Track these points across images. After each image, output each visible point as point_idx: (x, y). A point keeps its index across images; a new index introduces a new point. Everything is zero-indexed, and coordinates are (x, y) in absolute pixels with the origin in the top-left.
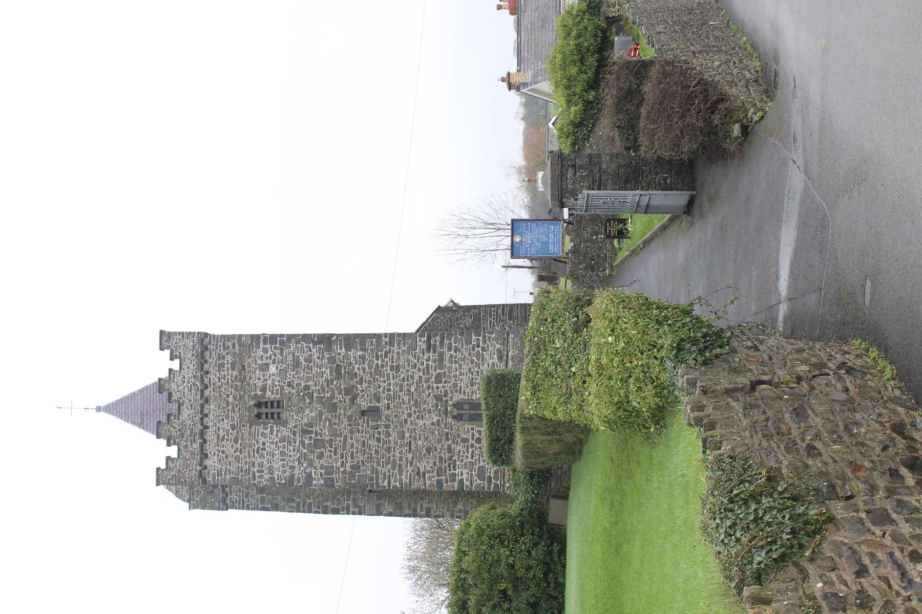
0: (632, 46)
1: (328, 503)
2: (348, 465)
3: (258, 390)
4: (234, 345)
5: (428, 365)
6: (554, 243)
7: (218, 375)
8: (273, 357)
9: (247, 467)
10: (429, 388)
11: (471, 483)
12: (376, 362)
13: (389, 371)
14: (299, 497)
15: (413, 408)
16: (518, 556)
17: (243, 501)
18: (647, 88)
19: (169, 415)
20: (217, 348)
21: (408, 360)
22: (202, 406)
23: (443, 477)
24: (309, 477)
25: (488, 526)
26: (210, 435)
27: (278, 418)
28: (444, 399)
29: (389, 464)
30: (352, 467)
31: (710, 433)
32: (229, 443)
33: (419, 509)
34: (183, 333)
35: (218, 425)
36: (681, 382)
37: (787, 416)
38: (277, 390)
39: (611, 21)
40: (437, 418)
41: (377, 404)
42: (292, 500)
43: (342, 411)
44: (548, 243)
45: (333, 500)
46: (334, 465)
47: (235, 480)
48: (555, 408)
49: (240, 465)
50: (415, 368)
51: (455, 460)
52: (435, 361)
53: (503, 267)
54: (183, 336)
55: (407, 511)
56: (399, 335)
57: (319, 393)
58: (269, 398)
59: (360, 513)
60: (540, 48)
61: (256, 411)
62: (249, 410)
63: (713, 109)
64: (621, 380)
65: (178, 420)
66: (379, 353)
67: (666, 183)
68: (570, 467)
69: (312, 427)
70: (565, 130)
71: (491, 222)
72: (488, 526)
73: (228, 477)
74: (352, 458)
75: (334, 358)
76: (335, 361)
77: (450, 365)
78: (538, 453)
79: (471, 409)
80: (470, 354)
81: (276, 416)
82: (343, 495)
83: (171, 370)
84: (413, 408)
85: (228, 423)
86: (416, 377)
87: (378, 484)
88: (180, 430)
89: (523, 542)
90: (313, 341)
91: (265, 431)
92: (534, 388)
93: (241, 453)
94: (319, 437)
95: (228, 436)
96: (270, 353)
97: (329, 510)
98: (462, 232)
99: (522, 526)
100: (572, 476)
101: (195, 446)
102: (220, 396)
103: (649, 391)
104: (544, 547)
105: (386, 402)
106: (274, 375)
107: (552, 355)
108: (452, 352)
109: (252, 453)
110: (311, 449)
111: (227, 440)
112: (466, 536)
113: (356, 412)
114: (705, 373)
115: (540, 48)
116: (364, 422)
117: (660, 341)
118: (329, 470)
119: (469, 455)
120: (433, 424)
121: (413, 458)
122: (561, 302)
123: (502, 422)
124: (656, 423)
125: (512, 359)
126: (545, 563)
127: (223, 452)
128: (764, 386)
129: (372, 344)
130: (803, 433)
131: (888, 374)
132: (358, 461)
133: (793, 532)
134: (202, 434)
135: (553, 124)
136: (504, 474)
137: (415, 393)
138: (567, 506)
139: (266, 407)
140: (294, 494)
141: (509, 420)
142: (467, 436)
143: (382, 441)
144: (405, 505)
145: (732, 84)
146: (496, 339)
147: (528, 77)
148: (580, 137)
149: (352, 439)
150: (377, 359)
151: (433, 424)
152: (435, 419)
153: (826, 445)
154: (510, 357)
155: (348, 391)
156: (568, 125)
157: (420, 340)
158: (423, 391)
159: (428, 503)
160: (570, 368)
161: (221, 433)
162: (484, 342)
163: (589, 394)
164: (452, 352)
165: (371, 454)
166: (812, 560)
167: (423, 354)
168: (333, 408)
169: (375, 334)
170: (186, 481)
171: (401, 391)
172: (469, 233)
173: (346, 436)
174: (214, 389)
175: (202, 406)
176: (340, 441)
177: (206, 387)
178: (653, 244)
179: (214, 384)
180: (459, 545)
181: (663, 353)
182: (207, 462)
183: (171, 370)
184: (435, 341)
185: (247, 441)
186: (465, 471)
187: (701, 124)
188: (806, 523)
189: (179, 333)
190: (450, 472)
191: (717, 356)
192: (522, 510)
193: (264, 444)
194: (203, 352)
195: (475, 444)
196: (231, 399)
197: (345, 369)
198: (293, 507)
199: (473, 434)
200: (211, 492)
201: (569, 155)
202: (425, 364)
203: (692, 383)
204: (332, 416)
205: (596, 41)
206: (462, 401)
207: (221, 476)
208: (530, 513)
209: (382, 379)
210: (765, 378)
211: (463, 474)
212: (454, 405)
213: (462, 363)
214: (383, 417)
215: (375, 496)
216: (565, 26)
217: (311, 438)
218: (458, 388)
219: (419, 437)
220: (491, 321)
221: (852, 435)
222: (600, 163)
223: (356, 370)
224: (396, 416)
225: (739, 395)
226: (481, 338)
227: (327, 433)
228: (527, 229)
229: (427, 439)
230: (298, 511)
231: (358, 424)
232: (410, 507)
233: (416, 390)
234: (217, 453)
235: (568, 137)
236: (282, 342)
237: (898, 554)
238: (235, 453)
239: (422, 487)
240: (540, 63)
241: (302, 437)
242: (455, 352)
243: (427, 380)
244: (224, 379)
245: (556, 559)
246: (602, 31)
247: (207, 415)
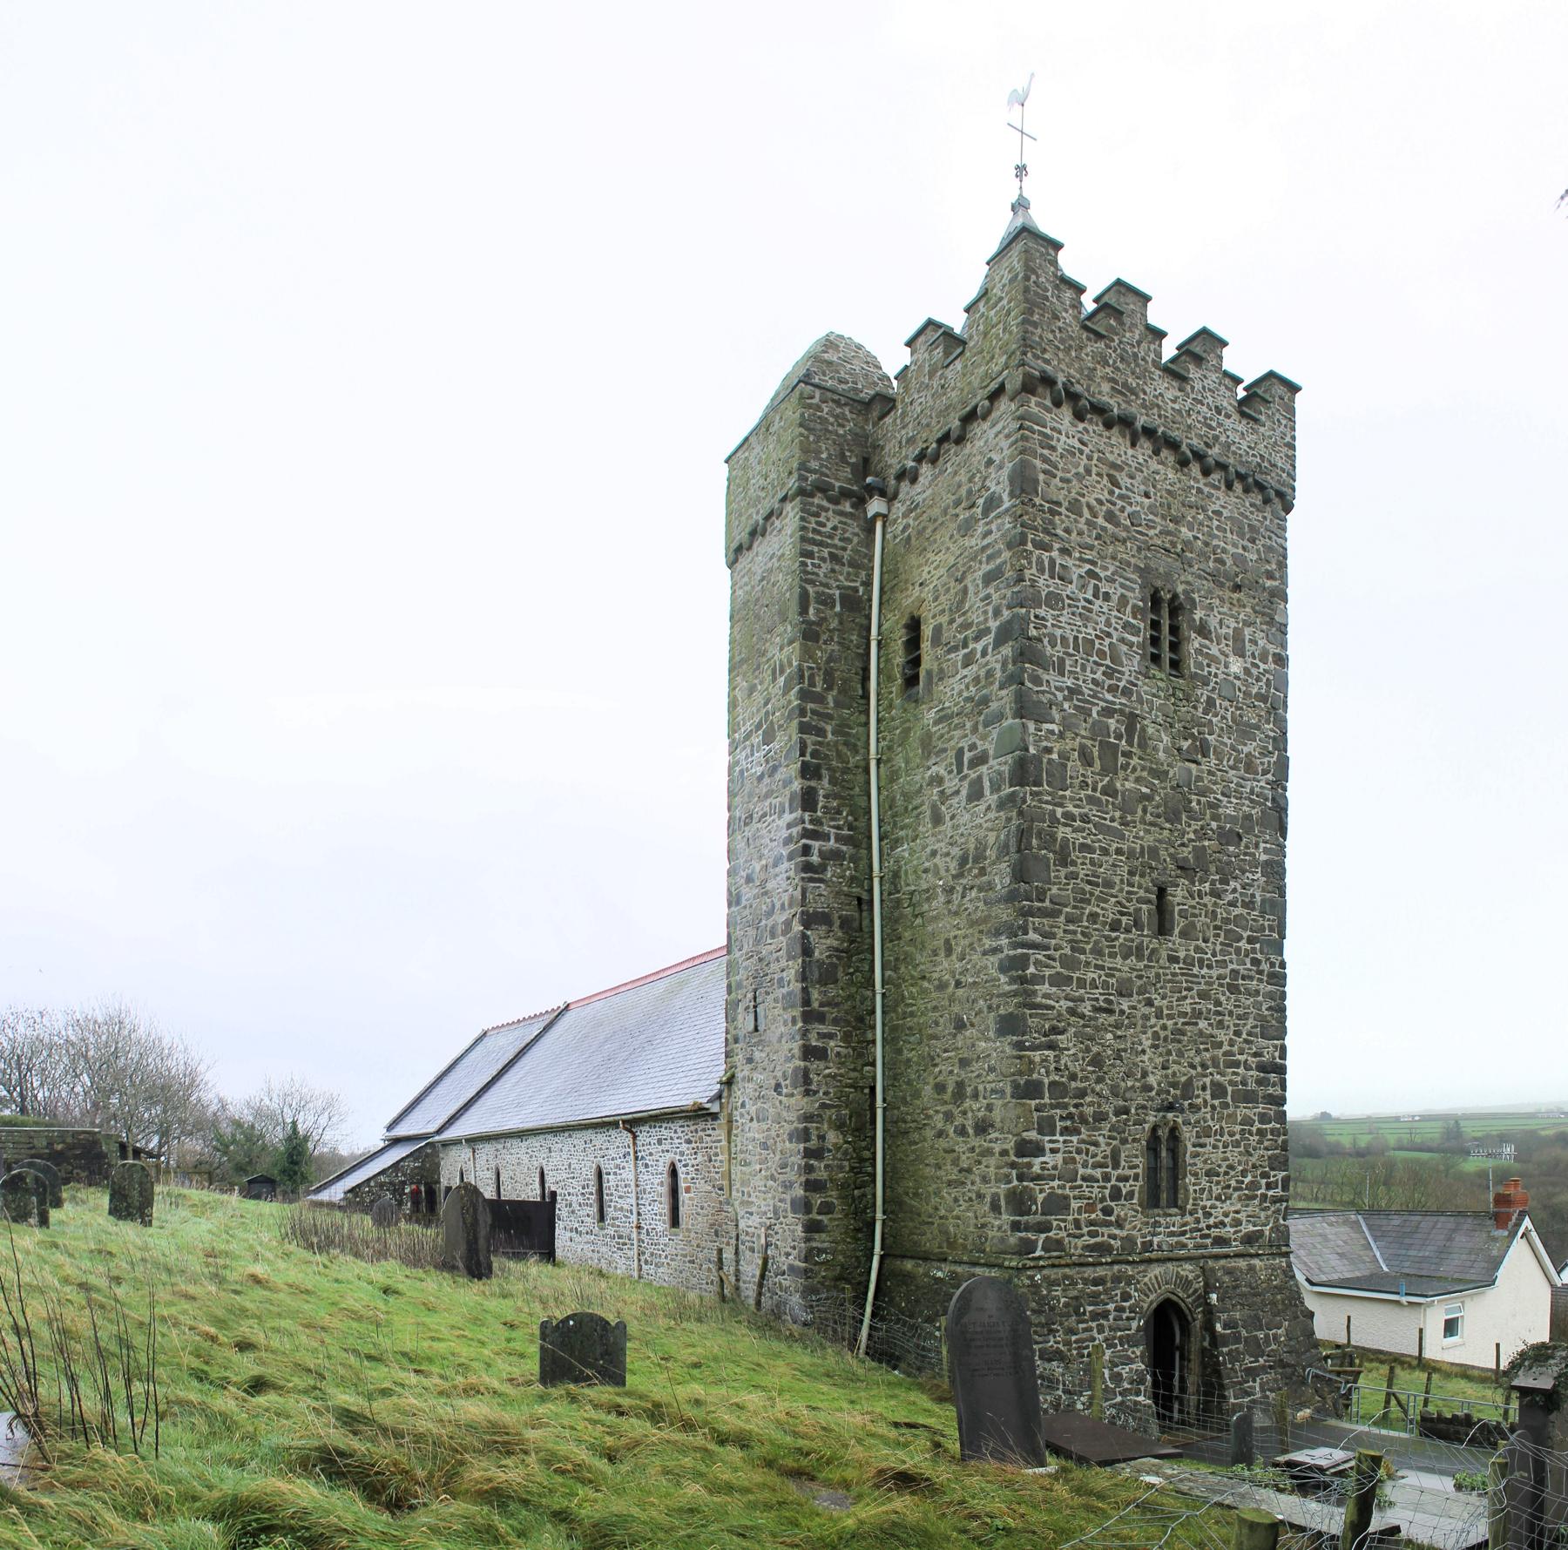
1: (825, 782)
11: (1038, 1178)
14: (838, 704)
28: (1186, 1103)
29: (1073, 949)
33: (824, 1029)
41: (1177, 931)
42: (829, 684)
46: (1068, 793)
51: (1079, 1133)
55: (815, 995)
73: (1038, 463)
77: (1239, 1118)
84: (1170, 1023)
86: (1222, 1036)
97: (813, 783)
101: (1106, 387)
119: (1089, 1171)
136: (1059, 1266)
142: (1123, 1163)
143: (1114, 935)
144: (833, 991)
159: (838, 1054)
165: (1088, 902)
190: (1057, 1118)
195: (1109, 1185)
202: (1240, 1057)
213: (1242, 1149)
219: (1120, 1037)
223: (1233, 884)
232: (829, 1004)
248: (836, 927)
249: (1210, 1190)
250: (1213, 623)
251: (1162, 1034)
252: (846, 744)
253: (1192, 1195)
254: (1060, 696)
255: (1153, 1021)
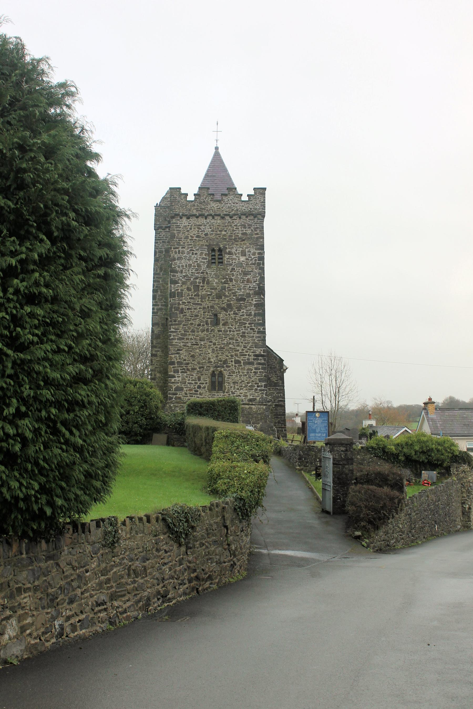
0: (430, 481)
1: (159, 293)
2: (184, 306)
3: (229, 250)
4: (257, 234)
5: (246, 355)
6: (315, 436)
7: (238, 224)
8: (250, 259)
9: (182, 244)
10: (232, 356)
12: (248, 323)
13: (242, 331)
14: (163, 275)
15: (219, 346)
16: (134, 416)
17: (160, 240)
18: (386, 489)
19: (213, 195)
20: (255, 223)
21: (248, 343)
22: (219, 215)
23: (176, 365)
24: (175, 282)
25: (151, 399)
26: (201, 221)
27: (213, 263)
28: (225, 365)
30: (182, 309)
31: (208, 509)
32: (197, 232)
33: (156, 349)
34: (265, 202)
35: (208, 225)
36: (228, 499)
37: (214, 538)
38: (229, 262)
39: (448, 469)
40: (213, 361)
41: (221, 324)
43: (216, 302)
44: (315, 432)
45: (161, 296)
47: (173, 236)
48: (218, 446)
49: (183, 239)
50: (244, 347)
52: (248, 359)
53: (314, 396)
54: (262, 202)
55: (155, 342)
56: (265, 337)
57: (228, 288)
58: (224, 257)
59: (153, 313)
60: (451, 423)
61: (216, 248)
62: (217, 245)
63: (370, 522)
64: (229, 476)
65: (210, 201)
66: (253, 325)
67: (338, 499)
68: (186, 447)
69: (207, 284)
70: (381, 443)
71: (340, 391)
72: (151, 399)
73: (175, 232)
74: (188, 309)
75: (250, 296)
76: (248, 297)
78: (195, 433)
79: (219, 382)
80: (253, 381)
81: (213, 261)
82: (165, 302)
83: (241, 195)
84: (219, 346)
85: (209, 231)
86: (238, 348)
87: (172, 325)
88: (204, 201)
89: (142, 419)
90: (260, 283)
91: (204, 255)
92: (227, 436)
93: (190, 240)
94: (200, 288)
95: (201, 231)
96: (253, 257)
98: (333, 372)
99: (151, 418)
100: (181, 448)
101: (195, 211)
102: (226, 226)
103: (224, 487)
104: (140, 432)
105: (223, 329)
106: (239, 259)
107: (241, 444)
108: (254, 370)
109: (190, 246)
110: (193, 283)
111: (198, 231)
112: (145, 386)
113: (216, 311)
114: (231, 508)
115: (451, 423)
116: (210, 316)
117: (244, 491)
118: (180, 295)
119: (190, 381)
120: (209, 359)
121: (188, 346)
122: (266, 449)
123: (211, 410)
124: (211, 491)
125: (250, 408)
126: (130, 432)
127: (191, 229)
128: (226, 531)
129: (258, 320)
130: (208, 543)
131: (231, 580)
132: (185, 313)
133: (177, 532)
134: (202, 215)
135: (406, 430)
137: (228, 347)
138: (162, 444)
139: (219, 255)
140: (165, 271)
141: (212, 413)
144: (159, 340)
145: (386, 533)
146: (262, 397)
147: (432, 415)
148: (376, 452)
149: (199, 308)
150: (249, 324)
151: (209, 359)
152: (212, 360)
153: (204, 550)
154: (251, 406)
155: (229, 306)
156: (384, 445)
157: (261, 350)
158: (229, 352)
160: (236, 453)
161: (202, 227)
162: (261, 390)
163: (224, 462)
164: (254, 370)
165: (190, 321)
166: (169, 536)
167: (253, 352)
168: (219, 296)
169: (265, 322)
170: (173, 206)
171: (230, 339)
172: (333, 376)
173: (201, 305)
174: (230, 222)
175: (219, 215)
176: (198, 301)
177: (231, 217)
178: (309, 493)
179: (233, 222)
180: (140, 382)
181: (239, 493)
182: (184, 219)
183: (241, 195)
184: (261, 360)
185: (198, 243)
186: (180, 379)
187: (362, 516)
188: (179, 537)
189: (265, 200)
191: (238, 514)
192: (160, 418)
193: (196, 254)
194: (252, 215)
196: (224, 233)
197: (243, 304)
198: (157, 271)
199: (203, 384)
200: (165, 220)
201: (352, 448)
203: (227, 503)
204: (214, 296)
205: (435, 460)
206: (223, 377)
207: (176, 228)
208: (159, 423)
209: (237, 327)
210: (229, 531)
211: (178, 378)
212: (221, 372)
214: (213, 328)
215: (164, 322)
216: (445, 442)
217: (200, 283)
218: (232, 374)
220: (274, 393)
221: (208, 560)
222: (348, 464)
223: (242, 311)
224: (214, 336)
225: (222, 521)
226: (263, 388)
227: (203, 293)
228: (323, 420)
229: (200, 355)
230: (154, 274)
231: (209, 312)
233: (230, 348)
234: (190, 225)
235: (377, 444)
236: (259, 264)
237: (171, 564)
238: (191, 236)
239: (170, 353)
240: (440, 423)
241: (201, 277)
242: (254, 372)
243: (236, 355)
244: (236, 229)
245: (132, 438)
246: (441, 464)
247: (213, 218)
248: (160, 326)
249: (235, 387)
250: (233, 251)
251: (215, 349)
252: (165, 283)
253: (227, 388)
254: (181, 278)
255: (212, 346)
